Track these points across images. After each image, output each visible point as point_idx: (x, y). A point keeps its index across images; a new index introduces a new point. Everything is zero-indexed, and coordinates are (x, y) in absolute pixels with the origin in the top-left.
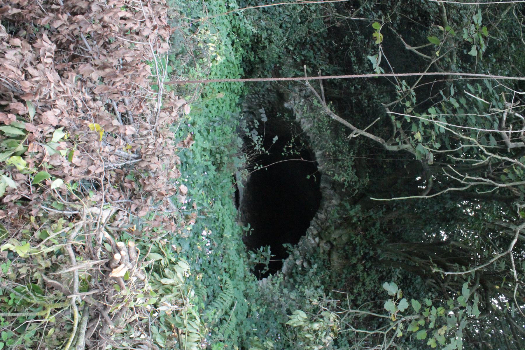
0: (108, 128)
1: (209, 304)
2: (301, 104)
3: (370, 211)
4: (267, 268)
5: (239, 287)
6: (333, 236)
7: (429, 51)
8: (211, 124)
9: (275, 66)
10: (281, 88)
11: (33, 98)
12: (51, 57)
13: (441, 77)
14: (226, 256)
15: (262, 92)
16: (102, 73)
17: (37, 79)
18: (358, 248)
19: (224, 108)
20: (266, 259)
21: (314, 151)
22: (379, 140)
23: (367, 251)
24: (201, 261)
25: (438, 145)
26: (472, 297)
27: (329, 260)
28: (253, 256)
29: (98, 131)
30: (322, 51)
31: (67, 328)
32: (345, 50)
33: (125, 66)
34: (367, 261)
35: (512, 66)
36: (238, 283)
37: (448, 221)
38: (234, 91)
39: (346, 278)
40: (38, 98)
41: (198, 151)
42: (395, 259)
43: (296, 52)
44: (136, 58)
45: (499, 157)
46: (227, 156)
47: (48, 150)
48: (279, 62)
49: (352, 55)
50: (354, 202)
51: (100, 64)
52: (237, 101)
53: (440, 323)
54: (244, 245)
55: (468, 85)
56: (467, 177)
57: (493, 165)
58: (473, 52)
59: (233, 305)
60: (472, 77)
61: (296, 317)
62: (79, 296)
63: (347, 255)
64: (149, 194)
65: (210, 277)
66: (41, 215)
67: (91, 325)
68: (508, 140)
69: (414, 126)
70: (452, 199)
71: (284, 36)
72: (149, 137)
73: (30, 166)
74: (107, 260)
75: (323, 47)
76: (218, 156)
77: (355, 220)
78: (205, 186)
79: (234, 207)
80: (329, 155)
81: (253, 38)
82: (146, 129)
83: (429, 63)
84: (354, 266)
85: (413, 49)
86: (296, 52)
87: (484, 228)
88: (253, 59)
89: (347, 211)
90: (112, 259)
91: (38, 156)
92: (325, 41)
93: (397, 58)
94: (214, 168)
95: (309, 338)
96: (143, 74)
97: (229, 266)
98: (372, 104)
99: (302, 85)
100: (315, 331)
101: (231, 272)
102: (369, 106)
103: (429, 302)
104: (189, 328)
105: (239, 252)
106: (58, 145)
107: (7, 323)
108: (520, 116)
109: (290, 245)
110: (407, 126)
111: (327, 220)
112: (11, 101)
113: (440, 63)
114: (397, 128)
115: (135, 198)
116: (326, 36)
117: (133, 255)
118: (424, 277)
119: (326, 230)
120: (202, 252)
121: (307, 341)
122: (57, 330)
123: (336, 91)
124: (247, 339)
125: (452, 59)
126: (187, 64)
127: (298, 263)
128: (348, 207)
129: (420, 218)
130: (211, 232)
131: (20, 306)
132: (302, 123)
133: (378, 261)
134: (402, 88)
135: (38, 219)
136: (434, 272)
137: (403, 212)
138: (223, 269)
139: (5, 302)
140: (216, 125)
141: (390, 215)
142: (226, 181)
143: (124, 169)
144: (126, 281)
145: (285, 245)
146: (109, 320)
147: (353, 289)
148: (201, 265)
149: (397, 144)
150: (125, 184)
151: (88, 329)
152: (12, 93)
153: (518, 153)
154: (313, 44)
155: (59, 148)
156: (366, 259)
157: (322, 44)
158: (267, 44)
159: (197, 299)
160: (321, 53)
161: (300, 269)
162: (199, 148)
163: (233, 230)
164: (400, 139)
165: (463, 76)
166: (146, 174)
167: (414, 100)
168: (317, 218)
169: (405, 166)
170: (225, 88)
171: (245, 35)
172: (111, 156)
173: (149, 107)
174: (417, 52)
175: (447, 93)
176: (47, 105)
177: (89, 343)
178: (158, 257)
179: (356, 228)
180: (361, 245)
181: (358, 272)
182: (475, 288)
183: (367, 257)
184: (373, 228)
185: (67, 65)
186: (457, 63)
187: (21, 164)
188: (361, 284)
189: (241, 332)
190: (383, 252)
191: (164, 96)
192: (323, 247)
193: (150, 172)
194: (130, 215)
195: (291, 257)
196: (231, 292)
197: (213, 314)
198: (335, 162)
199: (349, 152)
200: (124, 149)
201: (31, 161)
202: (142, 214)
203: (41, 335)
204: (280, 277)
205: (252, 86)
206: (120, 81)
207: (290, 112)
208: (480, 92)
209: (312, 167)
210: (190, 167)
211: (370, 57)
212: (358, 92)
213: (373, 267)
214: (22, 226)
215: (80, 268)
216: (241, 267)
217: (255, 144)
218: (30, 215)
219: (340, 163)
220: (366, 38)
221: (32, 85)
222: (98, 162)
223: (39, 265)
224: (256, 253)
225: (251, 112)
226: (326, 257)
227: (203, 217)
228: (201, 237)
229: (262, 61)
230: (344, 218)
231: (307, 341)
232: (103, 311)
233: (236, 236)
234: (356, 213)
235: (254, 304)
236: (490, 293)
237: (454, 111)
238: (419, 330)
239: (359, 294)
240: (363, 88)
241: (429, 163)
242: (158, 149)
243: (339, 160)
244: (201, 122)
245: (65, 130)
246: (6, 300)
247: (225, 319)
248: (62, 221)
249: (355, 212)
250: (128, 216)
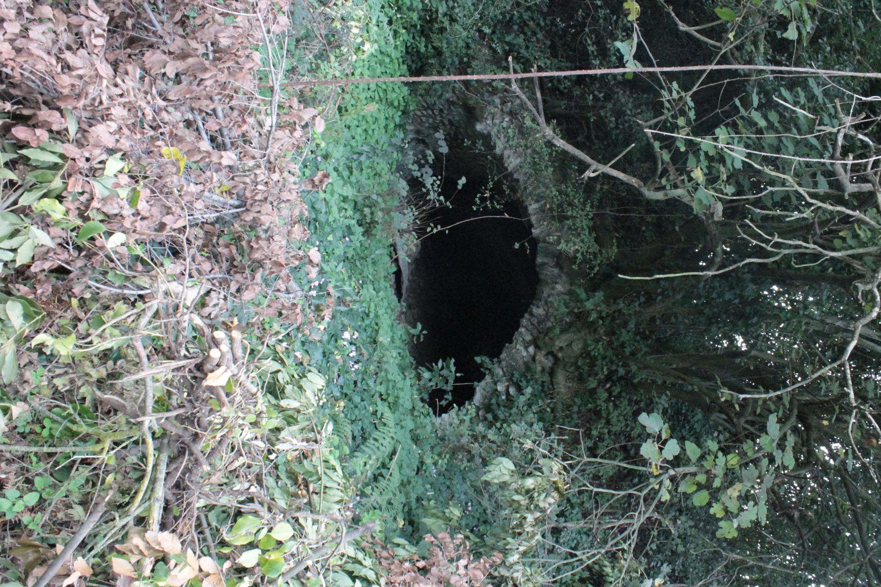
0: (193, 156)
1: (355, 449)
2: (505, 124)
3: (620, 301)
4: (449, 397)
5: (403, 423)
6: (558, 344)
7: (718, 33)
8: (355, 157)
9: (461, 62)
10: (471, 98)
11: (75, 103)
12: (101, 36)
13: (735, 73)
14: (383, 374)
15: (439, 106)
16: (181, 65)
17: (81, 72)
18: (599, 362)
19: (376, 132)
20: (447, 383)
21: (527, 203)
22: (634, 181)
23: (614, 368)
24: (341, 381)
25: (730, 189)
26: (784, 438)
27: (552, 383)
28: (426, 375)
29: (177, 160)
30: (540, 36)
31: (135, 475)
32: (577, 34)
33: (219, 53)
34: (614, 384)
35: (858, 57)
36: (402, 417)
37: (747, 317)
38: (392, 104)
39: (579, 412)
40: (81, 103)
41: (334, 201)
42: (660, 382)
43: (495, 37)
44: (237, 39)
45: (830, 208)
46: (382, 210)
47: (99, 190)
48: (467, 55)
49: (589, 42)
50: (592, 288)
51: (178, 52)
52: (397, 120)
53: (731, 477)
54: (412, 359)
55: (782, 90)
56: (777, 239)
57: (822, 224)
58: (791, 34)
59: (394, 453)
60: (789, 72)
61: (497, 469)
62: (153, 419)
63: (581, 374)
64: (260, 264)
65: (356, 407)
66: (88, 296)
67: (174, 466)
68: (844, 178)
69: (691, 161)
70: (754, 281)
71: (475, 10)
72: (258, 172)
73: (71, 213)
74: (199, 361)
75: (541, 29)
76: (367, 211)
77: (594, 316)
78: (346, 259)
79: (395, 298)
80: (551, 209)
81: (422, 14)
82: (254, 158)
83: (717, 53)
84: (593, 392)
85: (692, 30)
86: (495, 37)
87: (806, 331)
88: (423, 50)
89: (581, 301)
90: (207, 358)
91: (83, 199)
92: (545, 19)
93: (659, 39)
94: (359, 230)
95: (518, 502)
96: (248, 66)
97: (387, 389)
98: (623, 124)
99: (505, 92)
100: (528, 491)
101: (391, 399)
102: (617, 128)
103: (713, 446)
104: (325, 481)
105: (402, 369)
106: (115, 180)
107: (41, 464)
108: (866, 139)
109: (487, 360)
110: (679, 159)
111: (547, 316)
112: (40, 109)
113: (737, 54)
114: (663, 163)
115: (236, 272)
116: (545, 10)
117: (239, 353)
118: (708, 410)
119: (546, 334)
120: (344, 366)
121: (515, 505)
122: (119, 477)
123: (563, 104)
124: (417, 508)
125: (757, 47)
126: (315, 57)
127: (500, 388)
128: (583, 296)
129: (701, 313)
130: (356, 335)
131: (60, 439)
132: (505, 156)
133: (632, 384)
134: (671, 93)
135: (82, 300)
136: (723, 399)
137: (674, 304)
138: (377, 396)
139: (36, 433)
140: (363, 158)
141: (651, 309)
142: (381, 253)
143: (217, 226)
144: (228, 395)
145: (478, 359)
146: (202, 459)
147: (590, 430)
148: (342, 387)
149: (664, 188)
150: (220, 250)
151: (167, 474)
152: (39, 96)
153: (865, 200)
154: (523, 24)
155: (117, 185)
156: (613, 382)
157: (538, 25)
158: (446, 24)
159: (336, 440)
160: (538, 39)
161: (504, 397)
162: (336, 196)
163: (393, 335)
164: (668, 180)
165: (773, 72)
166: (253, 234)
167: (692, 115)
168: (531, 314)
169: (677, 228)
170: (377, 98)
171: (410, 9)
172: (202, 200)
173: (256, 126)
174: (698, 36)
175: (747, 104)
176: (97, 114)
177: (170, 497)
178: (276, 366)
179: (595, 331)
180: (604, 358)
181: (599, 402)
182: (789, 424)
183: (614, 378)
184: (623, 330)
185: (122, 54)
186: (765, 53)
187: (56, 210)
188: (603, 421)
189: (407, 495)
190: (639, 369)
191: (280, 107)
192: (541, 362)
193: (259, 229)
194: (230, 298)
195: (488, 378)
196: (392, 432)
197: (365, 463)
198: (560, 221)
199: (584, 204)
200: (217, 191)
201: (71, 206)
202: (247, 296)
203: (94, 485)
204: (470, 409)
205: (422, 96)
206: (211, 78)
207: (486, 138)
208: (802, 102)
209: (523, 230)
210: (322, 228)
211: (618, 44)
212: (600, 104)
213: (624, 394)
214: (60, 313)
215: (156, 375)
216: (408, 392)
217: (428, 191)
218: (70, 297)
219: (570, 222)
220: (613, 13)
221: (72, 81)
222: (176, 209)
223: (87, 374)
224: (430, 370)
225: (421, 140)
226: (546, 378)
227: (343, 308)
228: (341, 342)
229: (439, 52)
230: (576, 314)
231: (515, 505)
232: (191, 444)
233: (398, 343)
234: (596, 305)
235: (429, 453)
236: (814, 435)
237: (760, 131)
238: (698, 490)
239: (601, 438)
240: (608, 98)
241: (716, 219)
242: (273, 191)
243: (567, 218)
244: (338, 153)
245: (124, 157)
246: (37, 429)
247: (381, 475)
248: (120, 306)
249: (595, 303)
250: (225, 299)
